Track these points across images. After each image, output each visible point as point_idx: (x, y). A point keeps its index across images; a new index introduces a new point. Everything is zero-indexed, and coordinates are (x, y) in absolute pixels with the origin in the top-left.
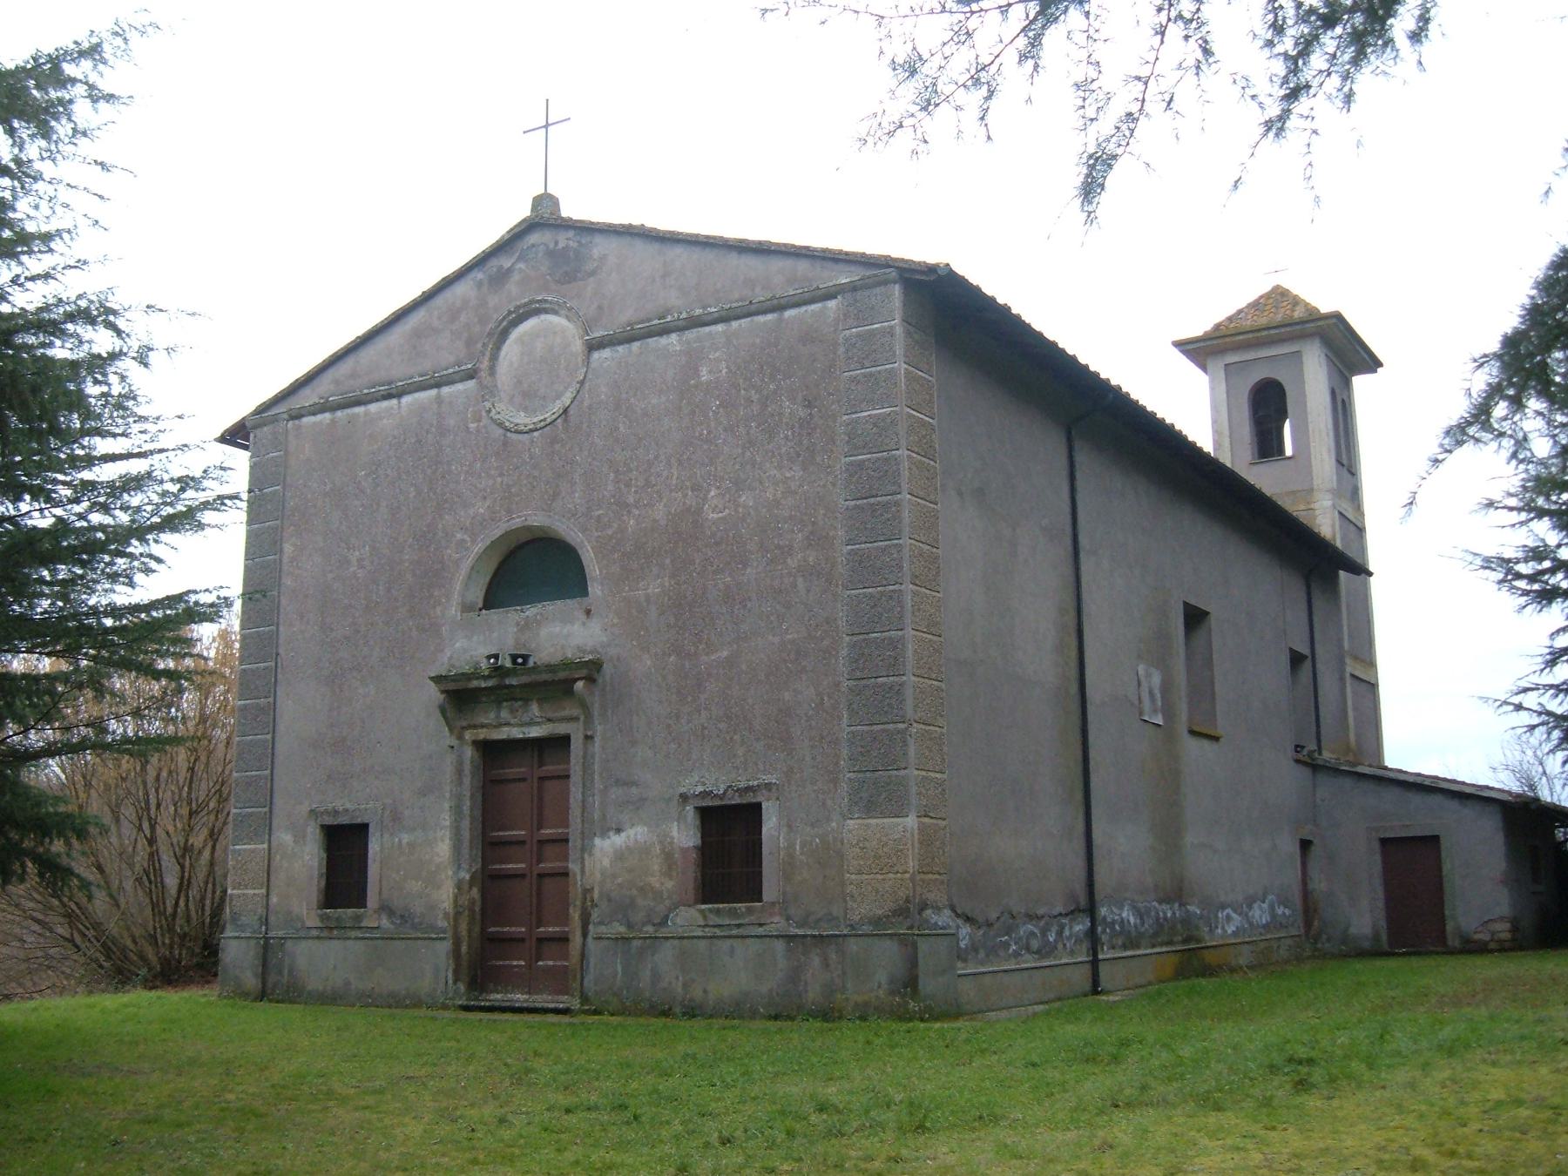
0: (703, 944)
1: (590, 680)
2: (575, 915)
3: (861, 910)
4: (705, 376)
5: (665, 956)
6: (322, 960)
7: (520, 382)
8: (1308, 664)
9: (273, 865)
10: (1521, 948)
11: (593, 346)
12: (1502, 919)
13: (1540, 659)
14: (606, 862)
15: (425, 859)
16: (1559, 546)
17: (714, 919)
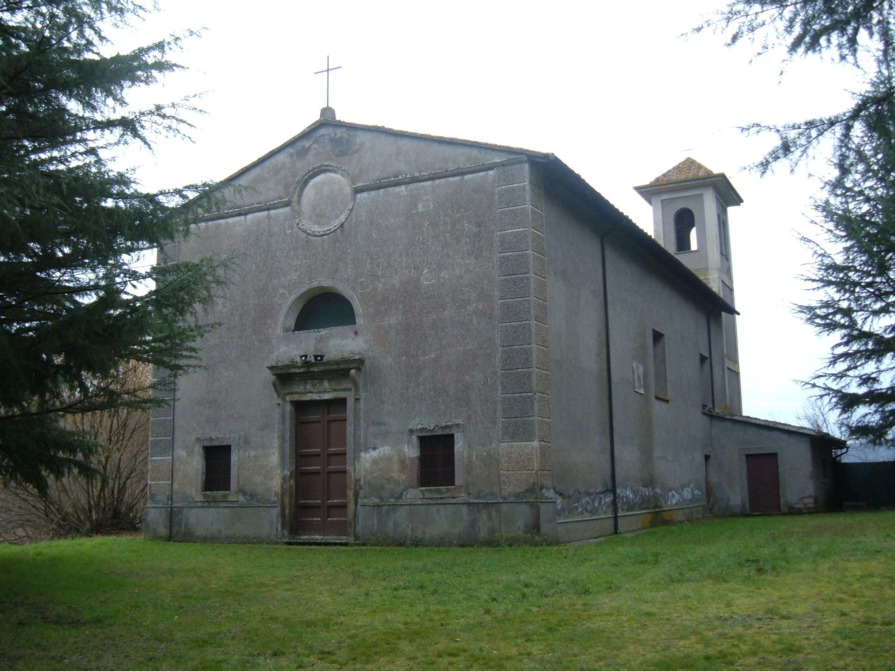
0: (422, 508)
1: (358, 369)
2: (350, 494)
3: (508, 490)
4: (420, 208)
5: (401, 515)
6: (204, 519)
7: (315, 209)
8: (708, 360)
9: (175, 468)
10: (818, 512)
11: (357, 191)
12: (810, 496)
13: (828, 360)
14: (367, 465)
15: (265, 464)
16: (839, 300)
17: (428, 495)
